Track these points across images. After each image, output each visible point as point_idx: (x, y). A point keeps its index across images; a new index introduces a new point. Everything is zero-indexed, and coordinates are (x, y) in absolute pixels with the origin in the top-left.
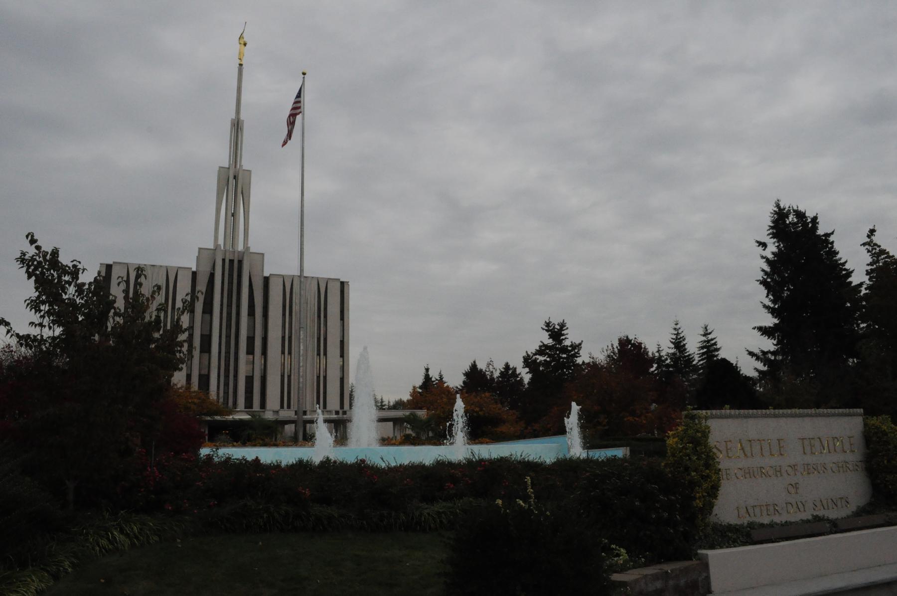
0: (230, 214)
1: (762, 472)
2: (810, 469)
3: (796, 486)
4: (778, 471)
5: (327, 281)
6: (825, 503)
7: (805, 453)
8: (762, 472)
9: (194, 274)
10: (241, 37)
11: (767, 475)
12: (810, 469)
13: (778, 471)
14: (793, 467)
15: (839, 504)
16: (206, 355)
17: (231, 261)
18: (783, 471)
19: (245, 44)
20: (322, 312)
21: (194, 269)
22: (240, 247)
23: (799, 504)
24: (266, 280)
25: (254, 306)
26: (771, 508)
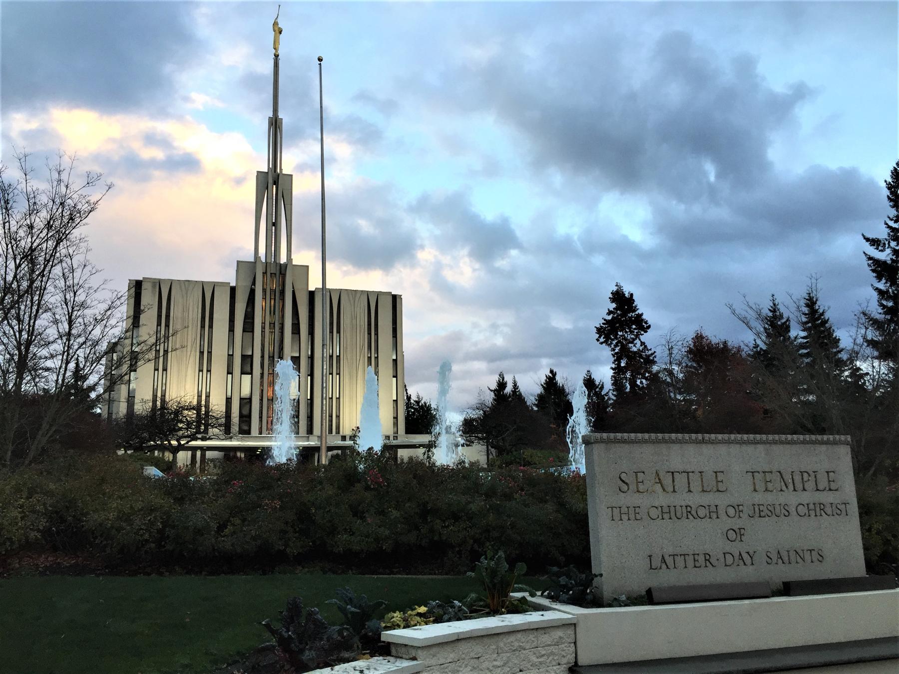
0: (270, 224)
1: (689, 512)
2: (759, 512)
3: (740, 533)
4: (713, 512)
5: (214, 285)
6: (784, 555)
7: (755, 490)
8: (689, 512)
9: (233, 290)
10: (275, 24)
11: (697, 517)
12: (759, 512)
13: (713, 512)
14: (738, 508)
15: (807, 556)
16: (230, 376)
18: (720, 512)
19: (280, 33)
21: (233, 284)
22: (283, 260)
23: (745, 556)
24: (312, 294)
25: (299, 324)
26: (701, 559)
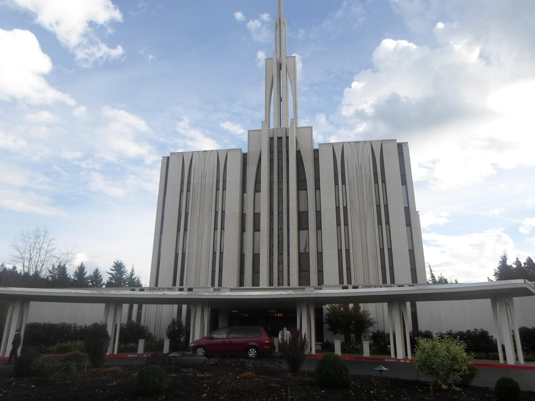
5: (382, 143)
17: (271, 139)
20: (379, 176)
24: (316, 151)
